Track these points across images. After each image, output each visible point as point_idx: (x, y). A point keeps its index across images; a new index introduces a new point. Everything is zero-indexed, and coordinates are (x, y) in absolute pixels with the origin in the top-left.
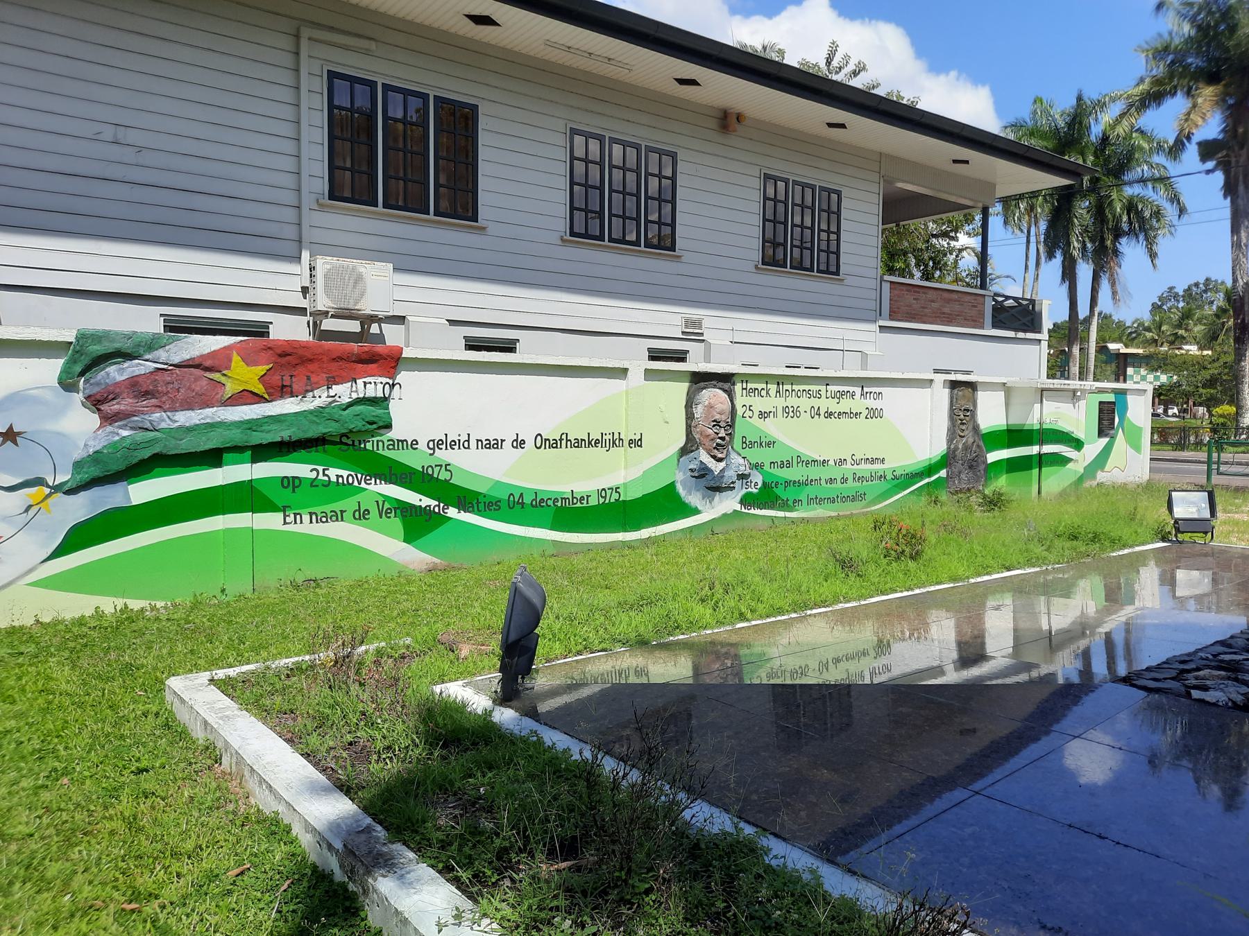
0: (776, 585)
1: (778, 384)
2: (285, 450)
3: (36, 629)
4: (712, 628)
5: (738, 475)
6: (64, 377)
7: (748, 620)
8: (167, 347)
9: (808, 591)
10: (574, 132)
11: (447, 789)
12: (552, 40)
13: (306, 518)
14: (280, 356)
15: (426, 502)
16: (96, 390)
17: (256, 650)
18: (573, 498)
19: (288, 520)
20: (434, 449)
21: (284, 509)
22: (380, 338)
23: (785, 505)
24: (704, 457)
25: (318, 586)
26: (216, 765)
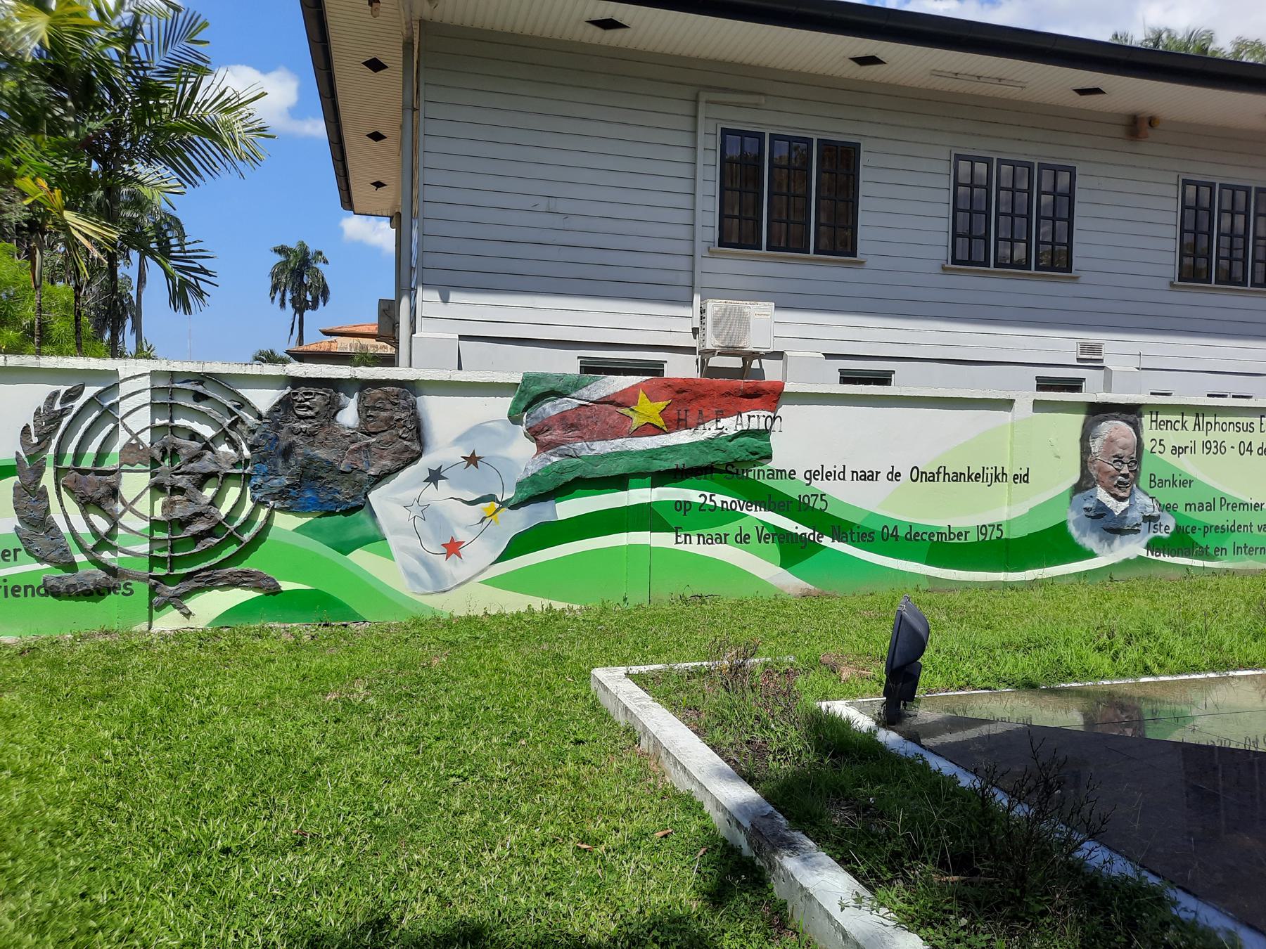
0: (1189, 640)
1: (1197, 415)
2: (678, 476)
3: (486, 619)
4: (1111, 679)
5: (1144, 517)
6: (512, 413)
7: (1154, 675)
8: (589, 387)
9: (1231, 650)
10: (959, 157)
11: (838, 793)
12: (939, 69)
13: (695, 539)
14: (678, 392)
15: (801, 529)
16: (535, 422)
17: (658, 653)
18: (950, 533)
19: (680, 540)
20: (810, 479)
21: (676, 530)
22: (760, 373)
23: (1203, 554)
24: (1102, 495)
25: (704, 602)
26: (636, 746)
